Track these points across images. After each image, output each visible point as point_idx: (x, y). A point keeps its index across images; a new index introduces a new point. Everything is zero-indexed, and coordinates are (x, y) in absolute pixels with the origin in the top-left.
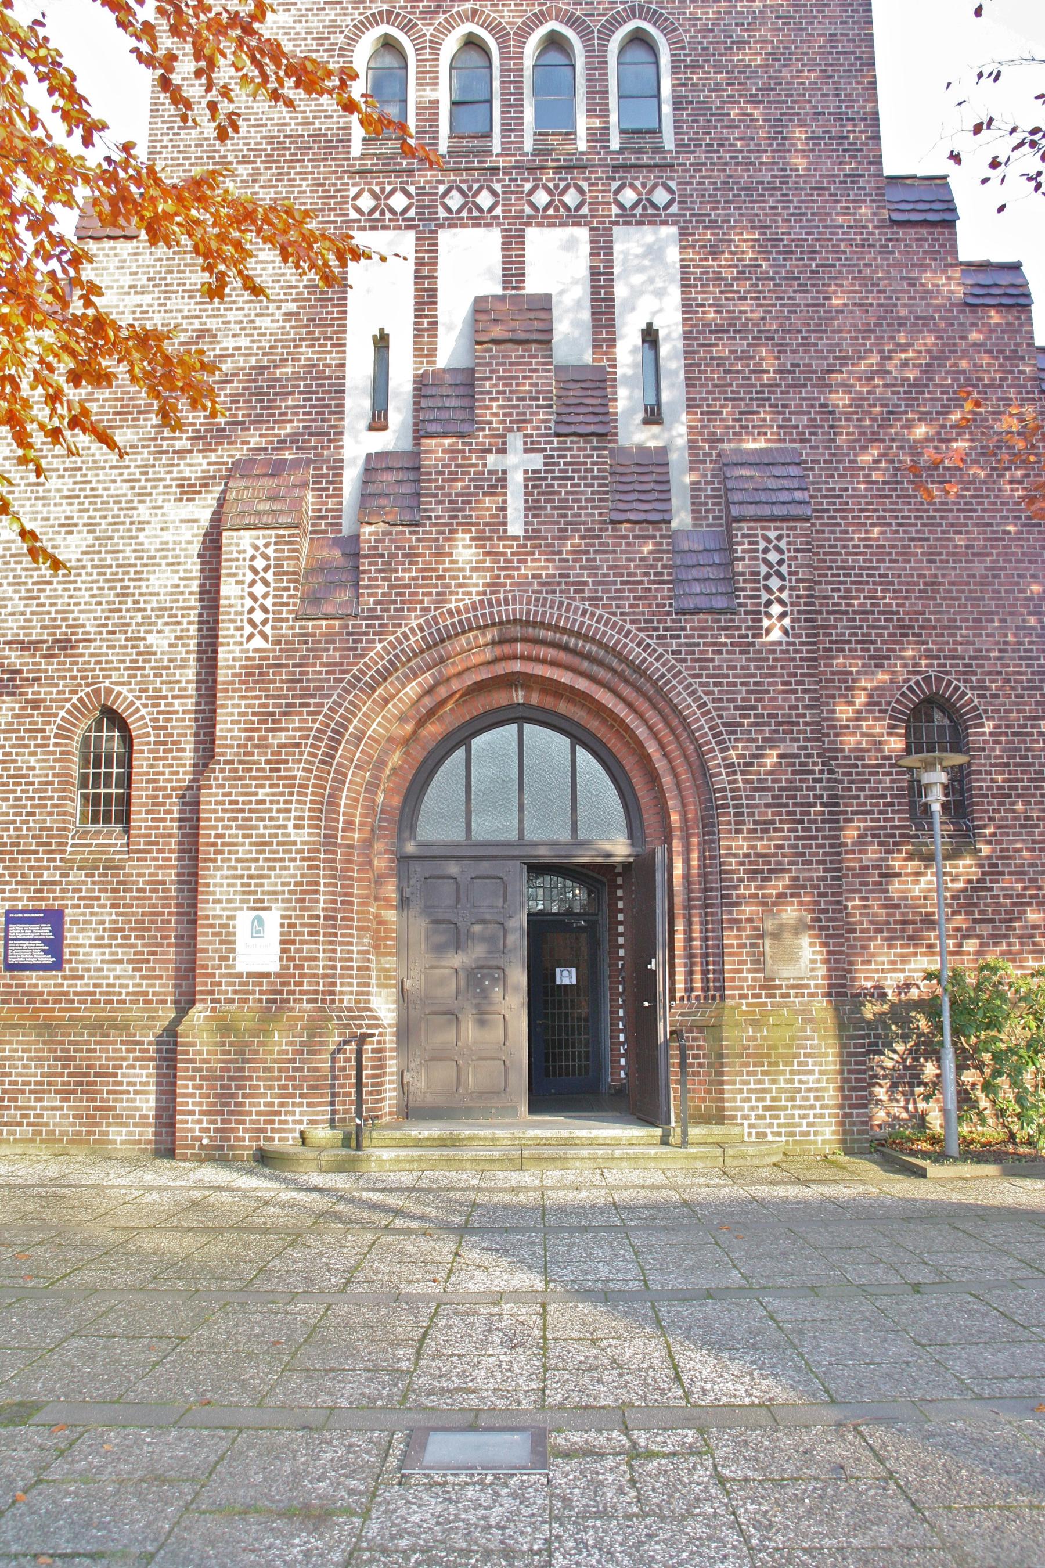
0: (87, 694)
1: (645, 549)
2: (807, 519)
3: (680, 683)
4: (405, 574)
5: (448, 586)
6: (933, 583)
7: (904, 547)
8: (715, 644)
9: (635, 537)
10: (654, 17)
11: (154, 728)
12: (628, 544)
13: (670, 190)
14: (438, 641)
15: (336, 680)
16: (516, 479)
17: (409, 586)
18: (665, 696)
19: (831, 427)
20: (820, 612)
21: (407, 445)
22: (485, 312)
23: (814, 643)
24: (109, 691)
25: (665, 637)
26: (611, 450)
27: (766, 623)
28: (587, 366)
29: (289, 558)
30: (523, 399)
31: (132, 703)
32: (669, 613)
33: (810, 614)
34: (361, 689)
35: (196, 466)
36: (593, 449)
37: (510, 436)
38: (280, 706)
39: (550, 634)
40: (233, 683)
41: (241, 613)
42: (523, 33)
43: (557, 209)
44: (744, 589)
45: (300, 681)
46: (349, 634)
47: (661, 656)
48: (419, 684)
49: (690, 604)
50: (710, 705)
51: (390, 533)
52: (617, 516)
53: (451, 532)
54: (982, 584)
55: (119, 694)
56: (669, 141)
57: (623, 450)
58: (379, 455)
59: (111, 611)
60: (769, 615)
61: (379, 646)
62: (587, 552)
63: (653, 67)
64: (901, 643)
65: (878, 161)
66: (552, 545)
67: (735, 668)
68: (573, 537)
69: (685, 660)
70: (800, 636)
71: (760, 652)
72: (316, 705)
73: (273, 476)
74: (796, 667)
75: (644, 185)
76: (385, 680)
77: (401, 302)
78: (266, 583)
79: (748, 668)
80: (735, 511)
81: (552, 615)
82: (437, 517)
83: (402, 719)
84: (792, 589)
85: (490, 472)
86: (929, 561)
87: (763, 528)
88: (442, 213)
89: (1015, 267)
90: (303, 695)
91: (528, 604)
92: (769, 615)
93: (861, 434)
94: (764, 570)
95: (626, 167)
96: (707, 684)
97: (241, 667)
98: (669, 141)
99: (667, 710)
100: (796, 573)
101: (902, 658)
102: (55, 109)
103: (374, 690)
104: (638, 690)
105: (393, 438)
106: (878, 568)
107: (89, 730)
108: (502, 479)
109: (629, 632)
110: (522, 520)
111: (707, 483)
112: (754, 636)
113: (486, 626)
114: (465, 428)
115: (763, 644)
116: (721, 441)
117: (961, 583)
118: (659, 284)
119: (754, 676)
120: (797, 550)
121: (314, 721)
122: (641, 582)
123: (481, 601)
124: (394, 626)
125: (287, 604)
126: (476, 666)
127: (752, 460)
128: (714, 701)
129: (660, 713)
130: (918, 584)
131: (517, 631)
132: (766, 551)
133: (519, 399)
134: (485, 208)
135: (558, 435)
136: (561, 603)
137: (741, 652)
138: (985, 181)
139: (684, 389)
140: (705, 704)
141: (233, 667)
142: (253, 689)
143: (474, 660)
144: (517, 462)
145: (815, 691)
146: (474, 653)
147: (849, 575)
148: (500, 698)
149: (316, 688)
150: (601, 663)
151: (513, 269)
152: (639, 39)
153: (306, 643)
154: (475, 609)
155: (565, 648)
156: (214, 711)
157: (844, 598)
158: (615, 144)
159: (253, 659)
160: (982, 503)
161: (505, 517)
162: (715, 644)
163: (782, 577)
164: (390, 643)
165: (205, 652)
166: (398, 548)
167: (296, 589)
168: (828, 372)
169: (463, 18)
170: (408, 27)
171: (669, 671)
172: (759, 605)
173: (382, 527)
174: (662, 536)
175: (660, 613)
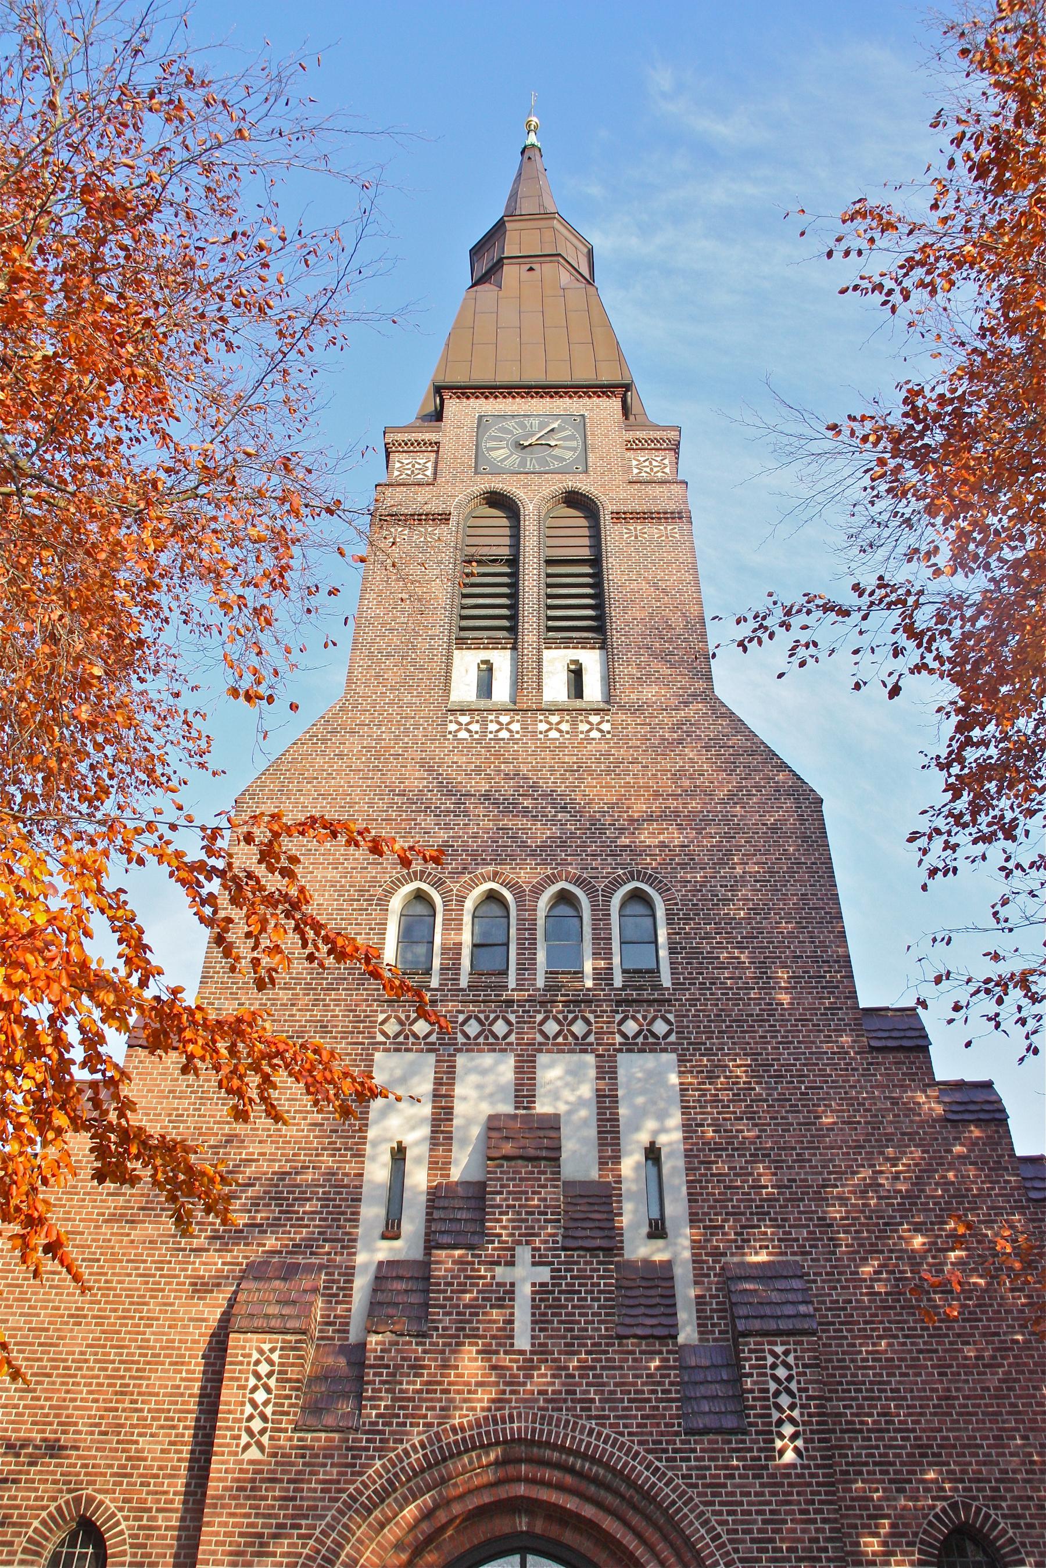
0: (67, 1502)
1: (652, 1365)
2: (813, 1333)
3: (692, 1511)
4: (411, 1385)
5: (452, 1400)
6: (947, 1398)
7: (912, 1359)
8: (726, 1467)
9: (642, 1352)
10: (650, 880)
11: (132, 1546)
12: (635, 1360)
13: (668, 1022)
14: (441, 1457)
15: (331, 1499)
16: (524, 1291)
17: (413, 1400)
18: (676, 1526)
19: (831, 1239)
20: (834, 1431)
21: (418, 1254)
22: (498, 1129)
23: (830, 1466)
24: (90, 1500)
25: (674, 1459)
26: (617, 1264)
27: (779, 1444)
28: (592, 1182)
29: (293, 1365)
30: (532, 1213)
31: (113, 1515)
32: (677, 1434)
33: (824, 1435)
34: (357, 1511)
35: (215, 1262)
36: (599, 1263)
37: (519, 1249)
38: (270, 1526)
39: (556, 1455)
40: (222, 1497)
41: (240, 1420)
42: (537, 891)
43: (565, 1038)
44: (754, 1407)
45: (294, 1499)
46: (348, 1449)
47: (671, 1480)
48: (418, 1507)
49: (700, 1423)
50: (725, 1537)
51: (397, 1343)
52: (622, 1331)
53: (458, 1344)
54: (997, 1397)
55: (101, 1503)
56: (666, 979)
57: (630, 1265)
58: (390, 1263)
59: (106, 1409)
60: (782, 1437)
61: (378, 1463)
62: (594, 1368)
63: (650, 920)
64: (920, 1464)
65: (853, 995)
66: (558, 1360)
67: (748, 1494)
68: (579, 1353)
69: (696, 1486)
70: (814, 1458)
71: (773, 1476)
72: (308, 1526)
73: (285, 1279)
74: (813, 1493)
75: (645, 1018)
76: (382, 1501)
77: (417, 1125)
78: (268, 1390)
79: (762, 1494)
80: (741, 1325)
81: (558, 1434)
82: (444, 1329)
83: (399, 1546)
84: (802, 1406)
85: (498, 1284)
86: (940, 1374)
87: (770, 1343)
88: (461, 1039)
89: (988, 1085)
90: (296, 1515)
91: (534, 1422)
92: (782, 1437)
93: (860, 1245)
94: (773, 1386)
95: (629, 1002)
96: (720, 1513)
97: (234, 1480)
98: (666, 981)
99: (679, 1542)
100: (806, 1390)
101: (924, 1481)
102: (120, 956)
103: (370, 1512)
104: (647, 1518)
105: (404, 1247)
106: (889, 1383)
107: (62, 1544)
108: (506, 1294)
109: (637, 1453)
110: (529, 1333)
111: (712, 1296)
112: (767, 1458)
113: (490, 1445)
114: (475, 1240)
115: (778, 1467)
116: (724, 1254)
117: (976, 1397)
118: (662, 1104)
119: (769, 1503)
120: (805, 1366)
121: (304, 1546)
122: (649, 1400)
123: (486, 1418)
124: (396, 1441)
125: (287, 1413)
126: (478, 1488)
127: (754, 1272)
128: (729, 1532)
129: (672, 1545)
130: (931, 1399)
131: (522, 1451)
132: (774, 1366)
133: (527, 1213)
134: (500, 1035)
135: (564, 1249)
136: (567, 1422)
137: (755, 1477)
138: (951, 1021)
139: (686, 1203)
140: (719, 1536)
141: (225, 1480)
142: (244, 1506)
143: (476, 1482)
144: (526, 1276)
145: (835, 1520)
146: (475, 1471)
147: (860, 1391)
148: (502, 1525)
149: (309, 1508)
150: (608, 1488)
151: (525, 1090)
152: (637, 897)
153: (303, 1456)
154: (479, 1426)
155: (571, 1470)
156: (199, 1529)
157: (857, 1415)
158: (618, 982)
159: (247, 1471)
160: (986, 1312)
161: (512, 1330)
162: (726, 1467)
163: (791, 1394)
164: (390, 1460)
165: (198, 1460)
166: (403, 1359)
167: (297, 1397)
168: (824, 1186)
169: (485, 879)
170: (438, 884)
171: (680, 1497)
172: (770, 1424)
173: (388, 1337)
174: (669, 1352)
175: (668, 1434)
